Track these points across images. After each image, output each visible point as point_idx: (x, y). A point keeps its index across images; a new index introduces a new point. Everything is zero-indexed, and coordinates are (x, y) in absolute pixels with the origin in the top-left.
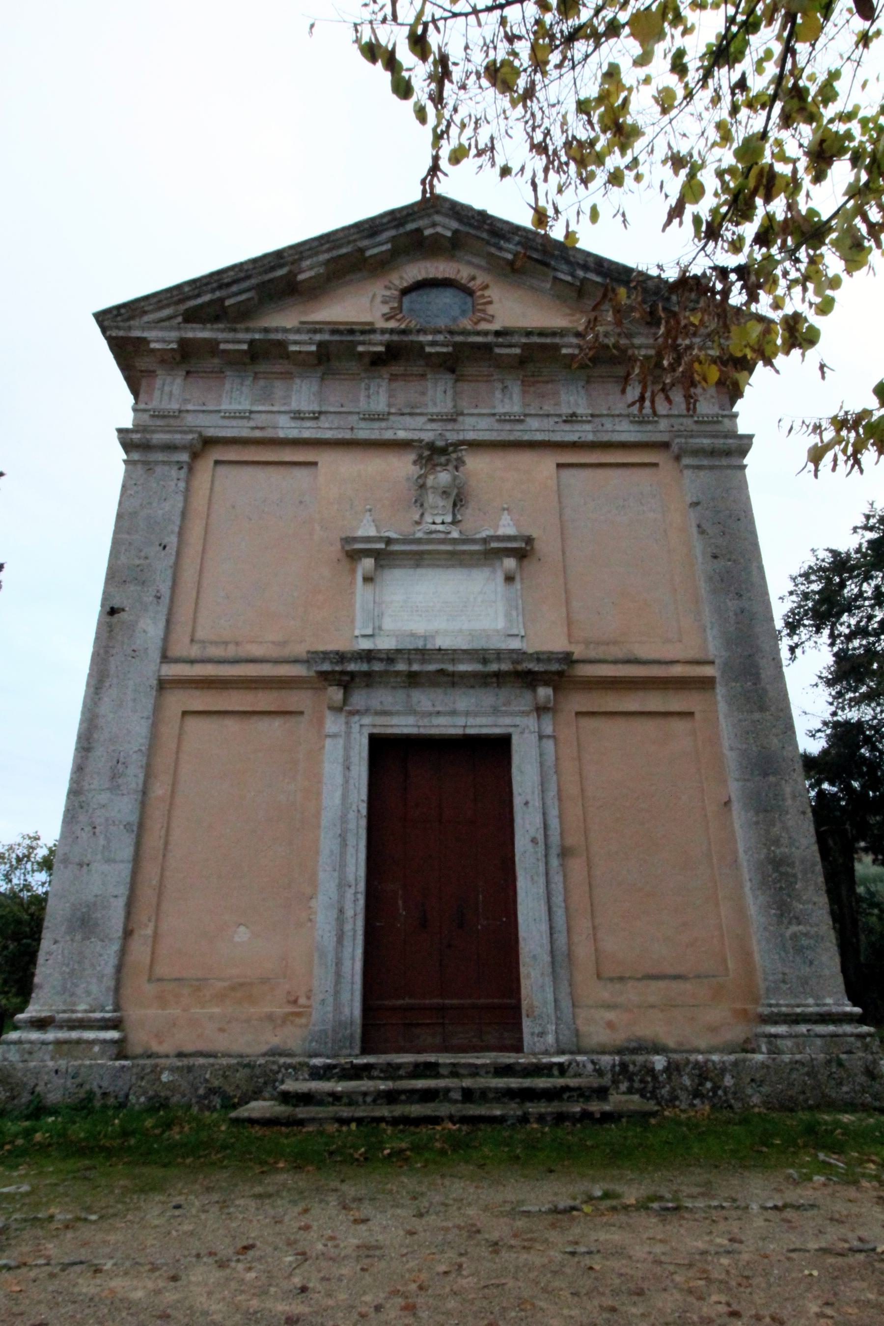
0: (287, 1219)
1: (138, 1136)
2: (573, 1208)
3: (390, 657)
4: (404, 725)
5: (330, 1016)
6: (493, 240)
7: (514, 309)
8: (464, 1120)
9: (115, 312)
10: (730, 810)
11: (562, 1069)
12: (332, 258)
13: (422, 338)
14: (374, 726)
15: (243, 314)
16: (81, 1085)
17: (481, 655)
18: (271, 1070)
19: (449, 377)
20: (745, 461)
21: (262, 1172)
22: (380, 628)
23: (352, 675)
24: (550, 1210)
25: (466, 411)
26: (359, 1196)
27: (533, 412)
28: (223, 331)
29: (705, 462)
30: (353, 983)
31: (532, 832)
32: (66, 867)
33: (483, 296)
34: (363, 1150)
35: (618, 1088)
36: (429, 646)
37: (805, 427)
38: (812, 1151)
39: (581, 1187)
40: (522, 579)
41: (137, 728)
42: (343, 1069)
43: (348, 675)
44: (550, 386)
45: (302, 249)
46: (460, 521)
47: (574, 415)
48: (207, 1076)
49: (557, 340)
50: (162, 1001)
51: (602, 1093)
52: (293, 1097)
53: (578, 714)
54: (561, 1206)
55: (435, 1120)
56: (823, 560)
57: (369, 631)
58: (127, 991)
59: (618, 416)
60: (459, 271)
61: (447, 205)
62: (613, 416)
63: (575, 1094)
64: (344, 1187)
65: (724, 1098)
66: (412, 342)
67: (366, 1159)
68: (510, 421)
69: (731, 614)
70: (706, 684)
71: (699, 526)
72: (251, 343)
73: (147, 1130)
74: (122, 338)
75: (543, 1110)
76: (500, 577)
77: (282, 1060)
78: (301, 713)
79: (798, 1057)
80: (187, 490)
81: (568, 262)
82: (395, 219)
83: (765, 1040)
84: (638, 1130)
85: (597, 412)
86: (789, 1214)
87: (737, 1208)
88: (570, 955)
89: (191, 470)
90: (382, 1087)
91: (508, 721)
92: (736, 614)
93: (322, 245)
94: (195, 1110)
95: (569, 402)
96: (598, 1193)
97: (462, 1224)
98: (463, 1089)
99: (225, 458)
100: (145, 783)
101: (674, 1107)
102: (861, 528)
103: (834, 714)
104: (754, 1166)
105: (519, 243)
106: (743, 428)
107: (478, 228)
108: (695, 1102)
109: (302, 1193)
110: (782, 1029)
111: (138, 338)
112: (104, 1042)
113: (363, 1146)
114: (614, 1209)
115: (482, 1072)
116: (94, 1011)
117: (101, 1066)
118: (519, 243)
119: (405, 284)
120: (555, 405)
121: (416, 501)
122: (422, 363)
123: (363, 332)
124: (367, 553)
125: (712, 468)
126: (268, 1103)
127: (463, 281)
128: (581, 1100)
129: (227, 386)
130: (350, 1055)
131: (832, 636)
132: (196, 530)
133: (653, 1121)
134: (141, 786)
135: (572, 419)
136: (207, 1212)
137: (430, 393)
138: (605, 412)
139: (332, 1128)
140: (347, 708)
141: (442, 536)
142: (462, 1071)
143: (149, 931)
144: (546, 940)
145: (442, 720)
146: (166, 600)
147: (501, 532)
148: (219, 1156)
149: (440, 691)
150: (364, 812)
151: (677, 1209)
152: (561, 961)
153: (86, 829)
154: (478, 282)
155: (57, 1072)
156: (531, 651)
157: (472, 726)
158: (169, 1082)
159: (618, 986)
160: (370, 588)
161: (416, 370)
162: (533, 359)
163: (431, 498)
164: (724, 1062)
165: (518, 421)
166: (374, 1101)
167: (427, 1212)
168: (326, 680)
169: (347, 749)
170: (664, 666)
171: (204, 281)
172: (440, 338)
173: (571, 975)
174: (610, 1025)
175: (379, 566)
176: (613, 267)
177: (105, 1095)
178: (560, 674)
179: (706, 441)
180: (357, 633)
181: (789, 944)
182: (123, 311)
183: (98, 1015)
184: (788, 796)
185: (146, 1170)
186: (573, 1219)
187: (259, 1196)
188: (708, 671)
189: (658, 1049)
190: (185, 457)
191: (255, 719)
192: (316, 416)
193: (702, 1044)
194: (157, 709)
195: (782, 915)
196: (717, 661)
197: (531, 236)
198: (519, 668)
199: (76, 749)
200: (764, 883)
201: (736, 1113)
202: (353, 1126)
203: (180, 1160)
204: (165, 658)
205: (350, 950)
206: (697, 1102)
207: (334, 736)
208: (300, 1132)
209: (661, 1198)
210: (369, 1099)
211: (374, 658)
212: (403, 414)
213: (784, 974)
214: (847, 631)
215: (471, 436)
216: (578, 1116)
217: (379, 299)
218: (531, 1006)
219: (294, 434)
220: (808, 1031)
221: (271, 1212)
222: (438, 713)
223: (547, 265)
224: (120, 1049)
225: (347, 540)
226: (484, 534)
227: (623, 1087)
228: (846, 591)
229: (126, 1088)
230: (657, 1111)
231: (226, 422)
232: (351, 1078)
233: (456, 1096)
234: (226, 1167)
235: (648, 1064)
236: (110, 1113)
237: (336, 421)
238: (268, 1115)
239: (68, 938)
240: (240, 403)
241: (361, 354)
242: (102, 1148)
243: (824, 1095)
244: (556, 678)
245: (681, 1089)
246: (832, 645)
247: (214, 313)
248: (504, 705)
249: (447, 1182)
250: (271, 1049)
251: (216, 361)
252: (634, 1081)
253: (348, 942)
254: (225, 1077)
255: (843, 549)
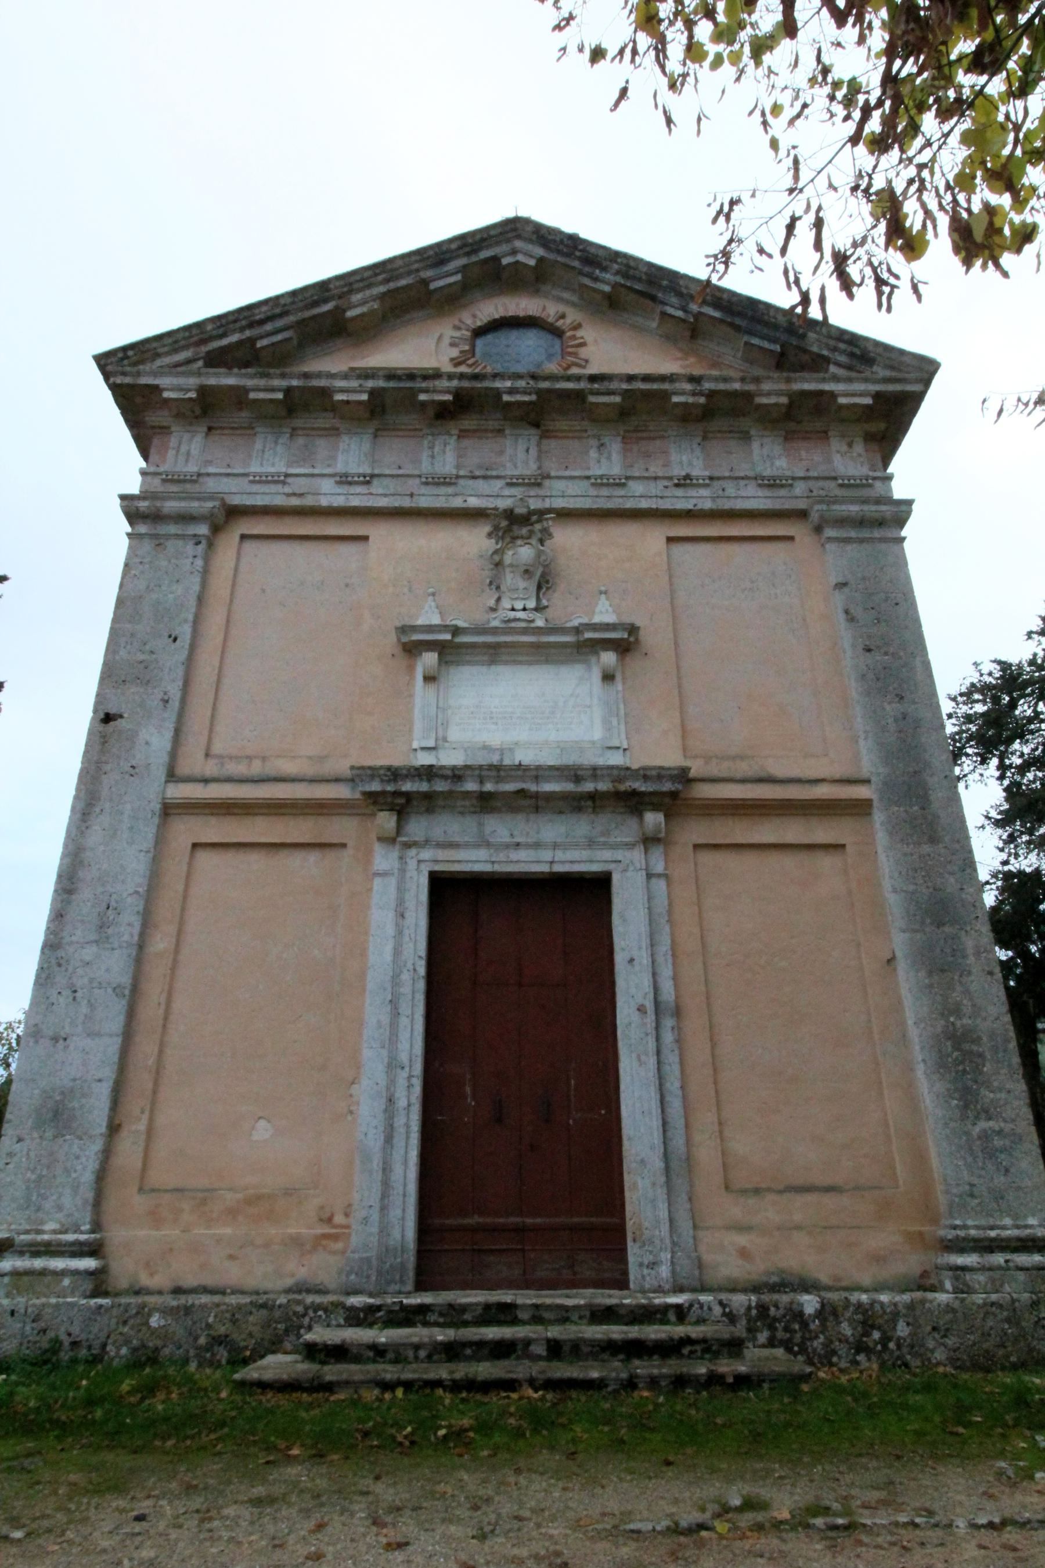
0: (291, 1539)
1: (107, 1406)
2: (702, 1527)
3: (456, 774)
4: (474, 860)
5: (375, 1239)
6: (587, 269)
7: (614, 352)
8: (550, 1385)
9: (120, 355)
10: (895, 970)
11: (681, 1313)
12: (389, 291)
13: (498, 384)
14: (436, 861)
15: (279, 358)
16: (44, 1331)
17: (574, 773)
18: (295, 1313)
19: (533, 431)
20: (903, 533)
21: (268, 1463)
22: (445, 740)
23: (408, 796)
24: (668, 1528)
25: (553, 474)
26: (398, 1503)
27: (637, 474)
28: (252, 376)
29: (853, 534)
30: (404, 1195)
31: (640, 1000)
32: (37, 1042)
33: (574, 337)
34: (409, 1429)
35: (755, 1339)
36: (507, 762)
37: (1021, 407)
38: (1028, 1433)
39: (712, 1489)
40: (624, 679)
41: (134, 863)
42: (390, 1312)
43: (403, 797)
44: (658, 442)
45: (352, 279)
46: (546, 607)
47: (688, 477)
48: (211, 1320)
49: (666, 386)
50: (155, 1218)
51: (734, 1347)
52: (321, 1351)
53: (697, 847)
54: (684, 1524)
55: (510, 1385)
56: (990, 674)
57: (431, 743)
58: (111, 1204)
59: (743, 478)
60: (544, 308)
61: (529, 228)
62: (737, 478)
63: (698, 1348)
64: (379, 1488)
65: (897, 1353)
66: (486, 388)
67: (412, 1443)
68: (608, 485)
69: (890, 721)
70: (861, 808)
71: (847, 612)
72: (288, 391)
73: (121, 1397)
74: (128, 385)
75: (655, 1371)
76: (596, 675)
77: (309, 1299)
78: (344, 846)
79: (994, 1297)
80: (205, 572)
81: (679, 294)
82: (465, 245)
83: (950, 1273)
84: (786, 1400)
85: (717, 474)
86: (1011, 1535)
87: (936, 1525)
88: (689, 1158)
89: (210, 545)
90: (440, 1338)
91: (607, 855)
92: (896, 720)
93: (376, 275)
94: (193, 1367)
95: (681, 463)
96: (737, 1502)
97: (543, 1552)
98: (549, 1341)
99: (255, 532)
100: (142, 934)
101: (831, 1365)
102: (1036, 633)
103: (1005, 863)
104: (950, 1456)
105: (618, 273)
106: (899, 490)
107: (567, 255)
108: (858, 1358)
109: (318, 1496)
110: (970, 1259)
111: (147, 386)
112: (76, 1273)
113: (410, 1423)
114: (759, 1527)
115: (575, 1317)
116: (66, 1232)
117: (72, 1305)
118: (618, 273)
119: (479, 324)
120: (664, 466)
121: (491, 583)
122: (499, 415)
123: (425, 378)
124: (430, 646)
125: (861, 541)
126: (289, 1358)
127: (550, 320)
128: (707, 1356)
129: (258, 445)
130: (400, 1293)
131: (1002, 767)
132: (215, 619)
133: (805, 1388)
134: (136, 938)
135: (685, 482)
136: (180, 1527)
137: (509, 451)
138: (727, 474)
139: (370, 1395)
140: (400, 839)
141: (523, 625)
142: (547, 1315)
143: (142, 1126)
144: (657, 1138)
145: (522, 855)
146: (175, 704)
147: (597, 619)
148: (212, 1436)
149: (520, 817)
150: (422, 971)
151: (846, 1528)
152: (677, 1168)
153: (64, 993)
154: (568, 320)
155: (12, 1313)
156: (635, 766)
157: (563, 862)
158: (160, 1327)
159: (752, 1201)
160: (432, 688)
161: (492, 424)
162: (637, 410)
163: (509, 579)
164: (895, 1305)
165: (618, 485)
166: (429, 1357)
167: (492, 1531)
168: (375, 803)
169: (401, 889)
170: (807, 786)
171: (231, 318)
172: (521, 384)
173: (691, 1186)
174: (744, 1253)
175: (443, 661)
176: (735, 299)
177: (75, 1344)
178: (674, 795)
179: (854, 508)
180: (415, 745)
181: (977, 1145)
182: (130, 353)
183: (70, 1237)
184: (970, 951)
185: (109, 1457)
186: (701, 1544)
187: (257, 1502)
188: (862, 792)
189: (807, 1286)
190: (203, 529)
191: (284, 853)
192: (367, 480)
193: (866, 1280)
194: (160, 840)
195: (966, 1106)
196: (873, 779)
197: (632, 264)
198: (622, 788)
199: (56, 891)
200: (941, 1065)
201: (915, 1375)
202: (400, 1393)
203: (158, 1443)
204: (172, 776)
205: (402, 1152)
206: (862, 1358)
207: (384, 874)
208: (327, 1400)
209: (826, 1511)
210: (422, 1354)
211: (437, 775)
212: (474, 478)
213: (972, 1185)
214: (1019, 761)
215: (559, 503)
216: (703, 1380)
217: (446, 341)
218: (640, 1227)
219: (339, 501)
220: (1007, 1261)
221: (271, 1529)
222: (518, 844)
223: (653, 298)
224: (98, 1283)
225: (403, 630)
226: (575, 623)
227: (763, 1337)
228: (1017, 712)
229: (103, 1336)
230: (811, 1373)
231: (255, 488)
232: (400, 1324)
233: (540, 1350)
234: (219, 1453)
235: (795, 1306)
236: (81, 1368)
237: (392, 485)
238: (285, 1377)
239: (35, 1135)
240: (273, 465)
241: (423, 404)
242: (56, 1423)
243: (1031, 1350)
244: (667, 800)
245: (840, 1341)
246: (1001, 778)
247: (242, 356)
248: (603, 834)
249: (523, 1481)
250: (297, 1284)
251: (244, 414)
252: (776, 1329)
253: (399, 1141)
254: (234, 1321)
255: (1014, 660)
